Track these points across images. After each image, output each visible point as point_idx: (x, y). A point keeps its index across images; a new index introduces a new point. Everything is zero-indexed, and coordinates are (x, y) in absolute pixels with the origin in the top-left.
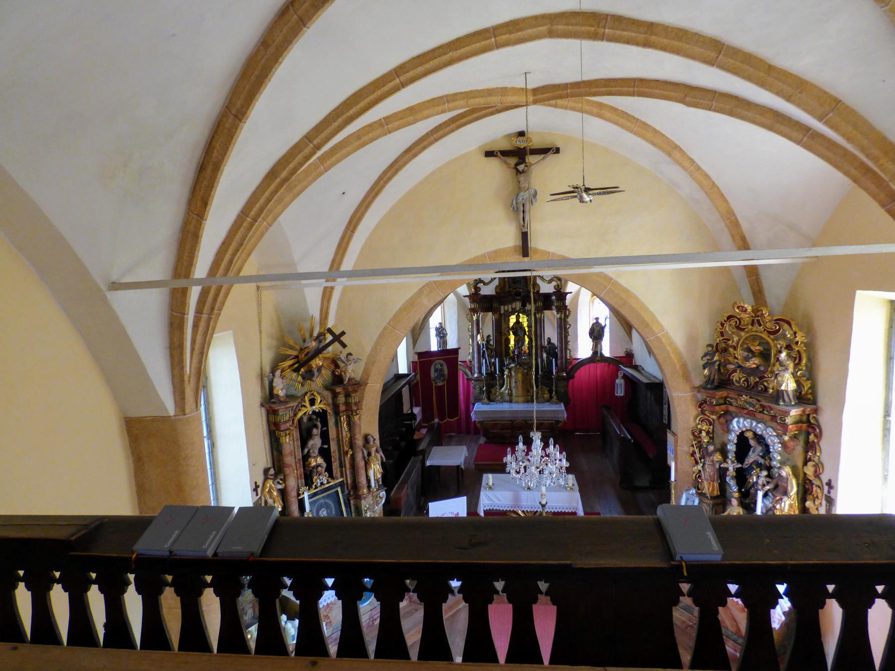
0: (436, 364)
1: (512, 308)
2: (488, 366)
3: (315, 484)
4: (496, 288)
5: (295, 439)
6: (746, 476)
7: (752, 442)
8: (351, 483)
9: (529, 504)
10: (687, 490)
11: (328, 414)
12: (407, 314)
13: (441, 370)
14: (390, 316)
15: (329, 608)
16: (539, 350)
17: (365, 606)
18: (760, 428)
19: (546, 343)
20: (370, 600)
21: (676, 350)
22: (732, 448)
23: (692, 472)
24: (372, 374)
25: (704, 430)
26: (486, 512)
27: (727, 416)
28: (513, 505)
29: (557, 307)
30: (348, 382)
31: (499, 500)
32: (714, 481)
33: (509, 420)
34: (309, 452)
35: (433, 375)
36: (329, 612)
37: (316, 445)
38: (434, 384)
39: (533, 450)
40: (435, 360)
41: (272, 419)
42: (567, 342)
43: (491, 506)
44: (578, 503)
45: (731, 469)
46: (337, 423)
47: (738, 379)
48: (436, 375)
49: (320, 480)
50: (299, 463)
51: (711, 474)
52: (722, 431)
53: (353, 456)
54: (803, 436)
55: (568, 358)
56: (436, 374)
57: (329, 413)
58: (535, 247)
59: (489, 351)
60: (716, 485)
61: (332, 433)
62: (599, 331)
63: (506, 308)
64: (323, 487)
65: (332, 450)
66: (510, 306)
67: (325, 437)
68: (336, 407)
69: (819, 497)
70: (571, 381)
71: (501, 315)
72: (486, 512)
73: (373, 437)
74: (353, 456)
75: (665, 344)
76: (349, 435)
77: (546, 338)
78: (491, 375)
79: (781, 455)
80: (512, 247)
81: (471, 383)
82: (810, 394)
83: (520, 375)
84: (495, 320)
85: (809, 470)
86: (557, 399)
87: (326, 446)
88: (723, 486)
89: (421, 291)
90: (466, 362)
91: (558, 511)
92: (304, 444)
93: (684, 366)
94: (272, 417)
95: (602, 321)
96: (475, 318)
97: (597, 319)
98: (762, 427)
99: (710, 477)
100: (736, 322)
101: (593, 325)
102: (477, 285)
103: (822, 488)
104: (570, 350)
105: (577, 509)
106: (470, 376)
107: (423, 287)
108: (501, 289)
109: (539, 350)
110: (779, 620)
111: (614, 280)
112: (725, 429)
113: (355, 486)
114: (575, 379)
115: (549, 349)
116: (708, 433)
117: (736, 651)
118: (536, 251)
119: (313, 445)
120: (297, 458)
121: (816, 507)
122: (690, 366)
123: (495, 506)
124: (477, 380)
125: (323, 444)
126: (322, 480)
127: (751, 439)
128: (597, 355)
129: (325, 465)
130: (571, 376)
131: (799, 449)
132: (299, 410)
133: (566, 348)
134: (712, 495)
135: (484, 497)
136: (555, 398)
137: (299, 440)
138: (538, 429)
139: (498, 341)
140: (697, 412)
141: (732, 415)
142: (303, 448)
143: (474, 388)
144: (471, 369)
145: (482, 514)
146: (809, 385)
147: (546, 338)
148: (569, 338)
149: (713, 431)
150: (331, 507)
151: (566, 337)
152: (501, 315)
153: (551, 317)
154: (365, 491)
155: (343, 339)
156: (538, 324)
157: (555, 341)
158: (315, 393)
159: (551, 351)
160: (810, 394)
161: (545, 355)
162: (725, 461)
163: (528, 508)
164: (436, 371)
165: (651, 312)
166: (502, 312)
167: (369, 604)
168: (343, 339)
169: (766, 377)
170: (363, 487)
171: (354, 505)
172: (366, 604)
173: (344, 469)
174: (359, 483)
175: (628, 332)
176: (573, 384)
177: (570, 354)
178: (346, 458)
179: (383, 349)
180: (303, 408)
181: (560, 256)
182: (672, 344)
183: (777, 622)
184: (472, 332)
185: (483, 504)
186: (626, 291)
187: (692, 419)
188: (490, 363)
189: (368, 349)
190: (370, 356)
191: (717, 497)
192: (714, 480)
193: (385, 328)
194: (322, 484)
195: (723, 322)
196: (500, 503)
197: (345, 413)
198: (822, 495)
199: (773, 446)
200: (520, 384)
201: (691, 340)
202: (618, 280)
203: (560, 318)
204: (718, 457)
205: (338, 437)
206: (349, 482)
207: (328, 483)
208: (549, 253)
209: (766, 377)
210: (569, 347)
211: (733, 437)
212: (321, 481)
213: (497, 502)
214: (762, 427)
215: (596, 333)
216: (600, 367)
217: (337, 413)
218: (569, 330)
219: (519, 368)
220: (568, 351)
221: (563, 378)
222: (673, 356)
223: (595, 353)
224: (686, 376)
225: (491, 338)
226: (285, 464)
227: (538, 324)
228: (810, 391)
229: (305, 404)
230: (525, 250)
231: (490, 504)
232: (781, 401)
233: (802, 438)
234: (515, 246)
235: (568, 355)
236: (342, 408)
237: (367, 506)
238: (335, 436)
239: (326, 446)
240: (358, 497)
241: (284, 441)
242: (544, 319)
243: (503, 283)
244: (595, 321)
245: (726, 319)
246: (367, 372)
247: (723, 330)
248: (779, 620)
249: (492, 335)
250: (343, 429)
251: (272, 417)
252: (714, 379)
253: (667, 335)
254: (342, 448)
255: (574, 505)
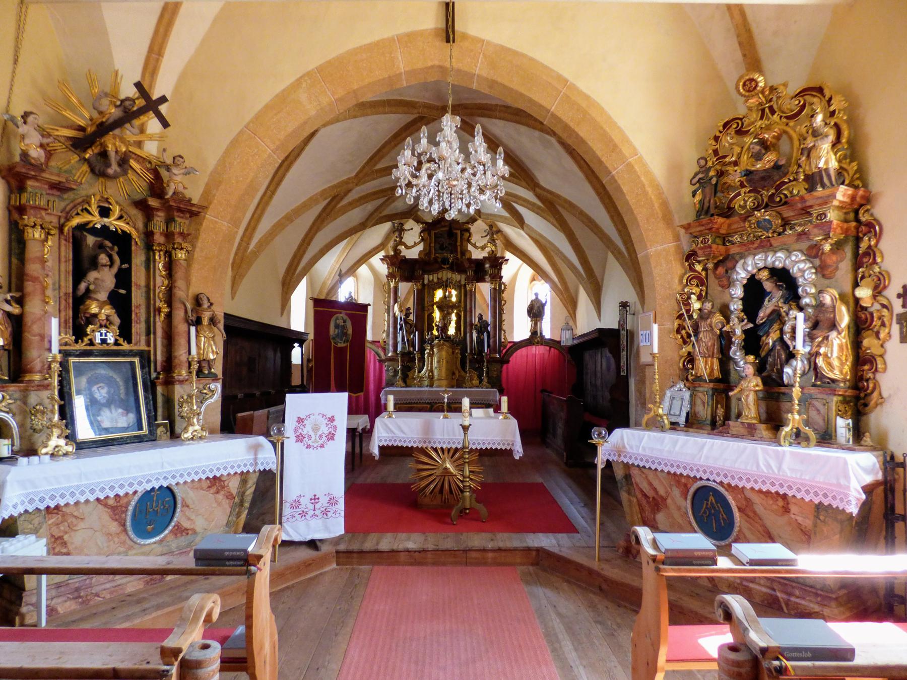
0: (337, 319)
1: (438, 279)
2: (405, 343)
3: (89, 337)
4: (421, 252)
5: (63, 259)
6: (761, 336)
7: (768, 286)
8: (163, 361)
9: (446, 437)
10: (671, 387)
11: (133, 243)
12: (276, 114)
13: (344, 327)
14: (249, 116)
15: (66, 524)
16: (468, 328)
17: (149, 544)
18: (778, 259)
19: (477, 320)
20: (162, 536)
21: (653, 181)
22: (736, 306)
23: (677, 359)
24: (215, 201)
25: (694, 294)
26: (382, 449)
27: (726, 263)
28: (423, 438)
29: (490, 275)
30: (172, 196)
31: (402, 432)
32: (713, 357)
33: (428, 403)
34: (88, 290)
35: (332, 331)
36: (66, 533)
37: (103, 281)
38: (333, 343)
39: (445, 128)
40: (337, 313)
41: (16, 201)
42: (501, 321)
43: (390, 441)
44: (514, 436)
45: (738, 332)
46: (149, 263)
47: (742, 203)
48: (336, 332)
49: (101, 335)
50: (66, 300)
51: (710, 344)
52: (720, 289)
53: (169, 316)
54: (850, 243)
55: (503, 340)
56: (337, 330)
57: (136, 243)
58: (463, 30)
59: (408, 326)
60: (716, 363)
61: (138, 276)
62: (539, 307)
63: (431, 277)
64: (105, 347)
65: (134, 301)
66: (435, 276)
67: (124, 278)
68: (148, 235)
69: (887, 323)
70: (505, 366)
71: (423, 285)
72: (382, 449)
73: (209, 300)
74: (169, 316)
75: (639, 173)
76: (166, 282)
77: (477, 314)
78: (407, 357)
79: (815, 286)
80: (431, 29)
81: (384, 366)
82: (857, 179)
83: (444, 353)
84: (417, 289)
85: (864, 293)
86: (488, 382)
87: (123, 291)
88: (725, 360)
89: (299, 81)
90: (379, 342)
91: (486, 448)
92: (79, 274)
93: (665, 205)
94: (16, 196)
95: (542, 298)
96: (392, 285)
97: (536, 295)
98: (783, 256)
99: (707, 350)
100: (738, 124)
101: (532, 301)
102: (397, 246)
103: (889, 307)
104: (504, 331)
105: (513, 445)
106: (383, 357)
107: (301, 77)
108: (426, 255)
109: (468, 328)
110: (858, 499)
111: (571, 83)
112: (725, 283)
113: (169, 365)
114: (510, 364)
115: (481, 326)
116: (699, 298)
117: (774, 590)
118: (465, 37)
119: (96, 279)
120: (63, 290)
121: (881, 342)
122: (673, 205)
123: (395, 441)
124: (391, 359)
125: (117, 286)
126: (106, 335)
127: (767, 280)
128: (535, 337)
129: (117, 320)
130: (504, 361)
131: (845, 267)
132: (78, 214)
133: (500, 329)
134: (711, 378)
135: (379, 425)
136: (486, 380)
137: (71, 262)
138: (454, 113)
139: (419, 316)
140: (683, 271)
141: (734, 258)
142: (77, 281)
143: (387, 370)
144: (384, 350)
145: (376, 451)
146: (855, 168)
147: (477, 314)
148: (504, 317)
149: (707, 293)
150: (115, 381)
151: (501, 315)
152: (423, 285)
153: (484, 289)
154: (184, 373)
155: (163, 108)
156: (468, 297)
157: (488, 318)
158: (112, 200)
159: (482, 327)
160: (857, 179)
161: (475, 334)
162: (728, 322)
163: (444, 443)
164: (337, 326)
165: (619, 127)
166: (426, 282)
167: (161, 541)
168: (163, 108)
169: (787, 183)
170: (180, 365)
171: (163, 395)
172: (153, 540)
173: (152, 336)
174: (175, 357)
175: (571, 312)
176: (507, 372)
177: (505, 336)
178: (157, 319)
179: (235, 163)
180: (86, 214)
181: (496, 45)
182: (648, 173)
183: (854, 502)
184: (389, 302)
185: (378, 437)
186: (587, 97)
187: (677, 281)
188: (408, 340)
189: (212, 161)
190: (215, 171)
191: (717, 380)
192: (713, 353)
193: (241, 132)
194: (104, 341)
195: (718, 134)
196: (404, 436)
197: (163, 248)
198: (892, 319)
199: (803, 276)
200: (444, 363)
201: (674, 168)
202: (575, 83)
203: (495, 289)
204: (718, 318)
205: (148, 286)
206: (159, 358)
207: (116, 343)
208: (483, 41)
209: (787, 183)
210: (504, 327)
211: (738, 292)
212: (103, 337)
213: (398, 433)
214: (783, 256)
215: (535, 311)
216: (537, 351)
217: (149, 247)
218: (505, 307)
219: (443, 344)
220: (503, 332)
221: (495, 360)
222: (649, 190)
223: (534, 333)
224: (667, 218)
225: (412, 311)
226: (27, 275)
227: (467, 297)
228: (857, 175)
229: (88, 208)
230: (449, 33)
231: (388, 437)
232: (819, 186)
233: (848, 251)
234: (437, 29)
235: (503, 337)
236: (159, 238)
237: (185, 397)
238: (142, 283)
239: (123, 291)
240: (169, 382)
241: (31, 235)
242: (475, 292)
243: (428, 249)
244: (534, 297)
245: (721, 128)
246: (207, 193)
247: (718, 146)
248: (858, 499)
249: (412, 308)
250: (157, 272)
251: (16, 196)
252: (709, 207)
253: (644, 165)
254: (152, 302)
255: (509, 438)
